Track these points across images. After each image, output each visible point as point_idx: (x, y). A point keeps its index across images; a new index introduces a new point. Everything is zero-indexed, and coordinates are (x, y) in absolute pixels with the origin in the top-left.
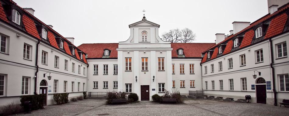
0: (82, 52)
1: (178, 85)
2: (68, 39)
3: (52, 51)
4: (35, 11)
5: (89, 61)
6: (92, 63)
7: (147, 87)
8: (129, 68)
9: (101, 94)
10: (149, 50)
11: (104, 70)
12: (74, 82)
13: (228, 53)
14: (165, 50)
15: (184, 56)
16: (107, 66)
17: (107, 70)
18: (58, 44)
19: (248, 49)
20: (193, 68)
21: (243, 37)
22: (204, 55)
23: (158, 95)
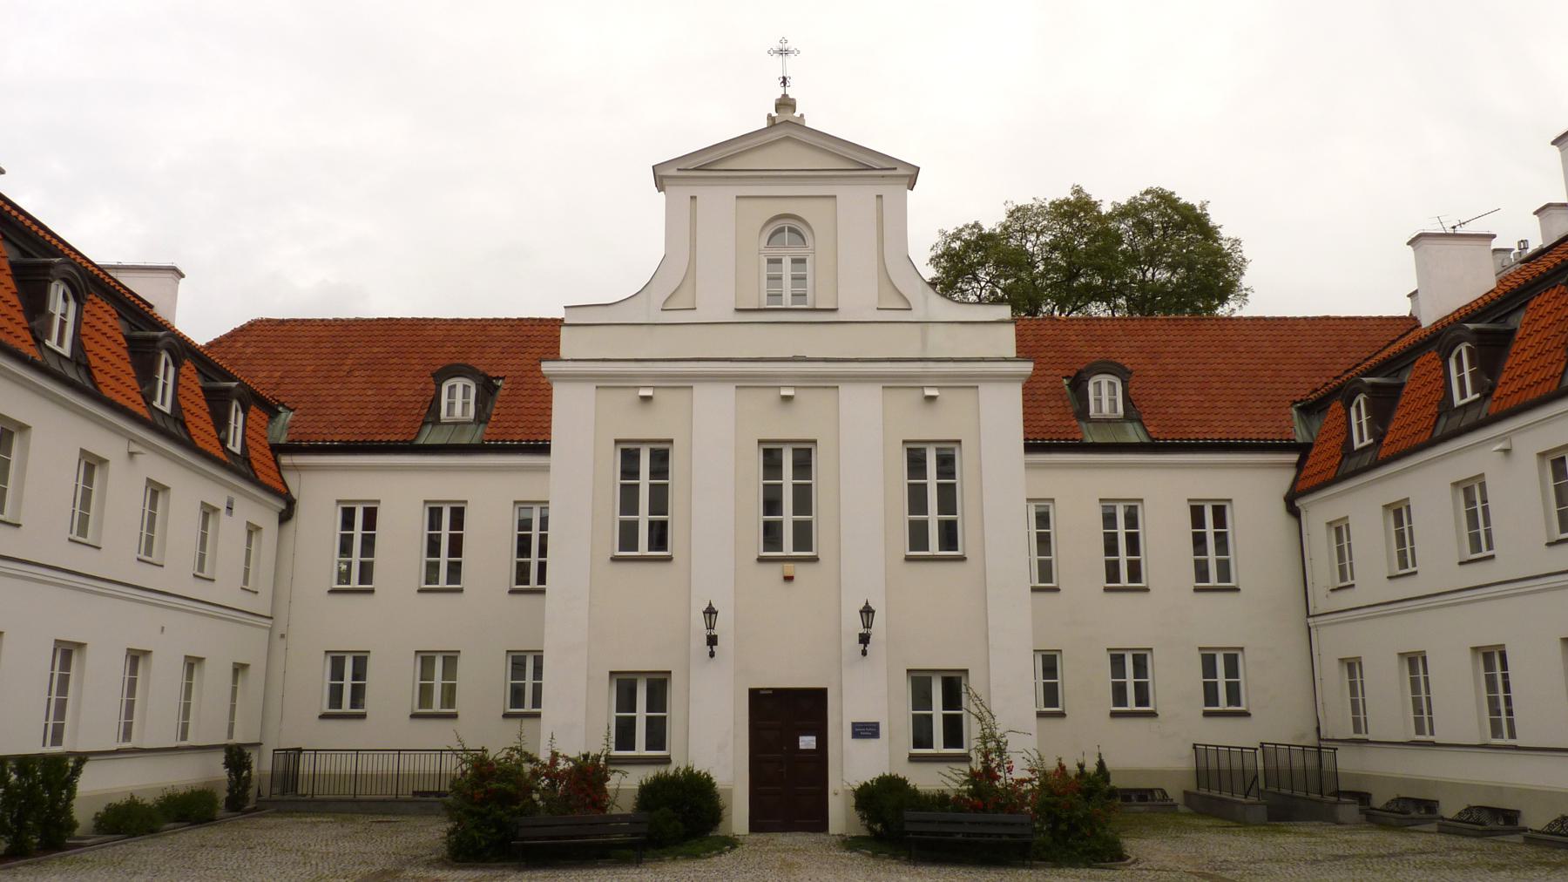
0: (242, 385)
1: (1087, 683)
2: (127, 280)
3: (135, 448)
4: (182, 276)
5: (295, 468)
6: (324, 487)
7: (806, 707)
8: (646, 533)
9: (386, 765)
10: (828, 378)
11: (433, 547)
12: (147, 653)
13: (1532, 395)
14: (967, 377)
15: (1134, 434)
16: (458, 516)
17: (456, 546)
18: (30, 318)
19: (1502, 437)
20: (1221, 541)
21: (1513, 332)
22: (1317, 425)
23: (904, 782)
